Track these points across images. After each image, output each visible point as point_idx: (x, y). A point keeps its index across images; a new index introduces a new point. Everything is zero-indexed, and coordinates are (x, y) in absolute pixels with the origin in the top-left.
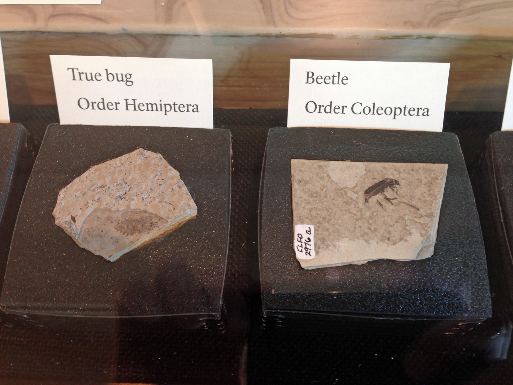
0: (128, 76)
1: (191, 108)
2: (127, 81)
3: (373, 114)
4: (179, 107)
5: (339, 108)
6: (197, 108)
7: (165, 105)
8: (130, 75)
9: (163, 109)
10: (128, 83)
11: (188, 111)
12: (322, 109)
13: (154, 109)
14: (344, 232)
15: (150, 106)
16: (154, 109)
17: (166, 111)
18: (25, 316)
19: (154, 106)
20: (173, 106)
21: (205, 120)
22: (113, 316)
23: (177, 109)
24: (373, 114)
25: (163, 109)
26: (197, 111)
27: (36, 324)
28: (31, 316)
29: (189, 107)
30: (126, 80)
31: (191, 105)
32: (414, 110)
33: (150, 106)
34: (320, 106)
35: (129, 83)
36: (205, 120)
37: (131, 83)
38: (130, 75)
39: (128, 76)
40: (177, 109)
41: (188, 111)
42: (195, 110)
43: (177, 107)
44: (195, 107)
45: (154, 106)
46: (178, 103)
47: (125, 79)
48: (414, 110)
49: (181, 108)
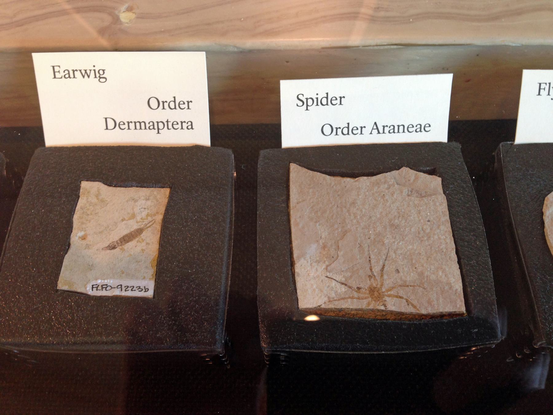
0: (101, 72)
1: (185, 125)
2: (100, 78)
3: (317, 105)
4: (173, 124)
5: (357, 129)
6: (192, 125)
7: (158, 122)
8: (103, 70)
9: (156, 127)
10: (101, 80)
11: (182, 128)
12: (339, 131)
13: (143, 127)
14: (373, 260)
15: (138, 124)
16: (143, 127)
17: (158, 129)
18: (16, 351)
19: (143, 124)
20: (166, 124)
21: (201, 136)
22: (121, 349)
23: (170, 127)
24: (317, 105)
25: (156, 127)
26: (192, 128)
27: (29, 359)
28: (21, 352)
29: (184, 124)
30: (99, 76)
31: (185, 122)
32: (336, 99)
33: (138, 124)
34: (337, 128)
35: (102, 80)
36: (201, 136)
37: (104, 80)
38: (103, 70)
39: (101, 72)
40: (170, 127)
41: (182, 128)
42: (190, 127)
43: (170, 124)
44: (190, 123)
45: (143, 124)
46: (171, 120)
47: (98, 75)
48: (336, 99)
49: (174, 126)
